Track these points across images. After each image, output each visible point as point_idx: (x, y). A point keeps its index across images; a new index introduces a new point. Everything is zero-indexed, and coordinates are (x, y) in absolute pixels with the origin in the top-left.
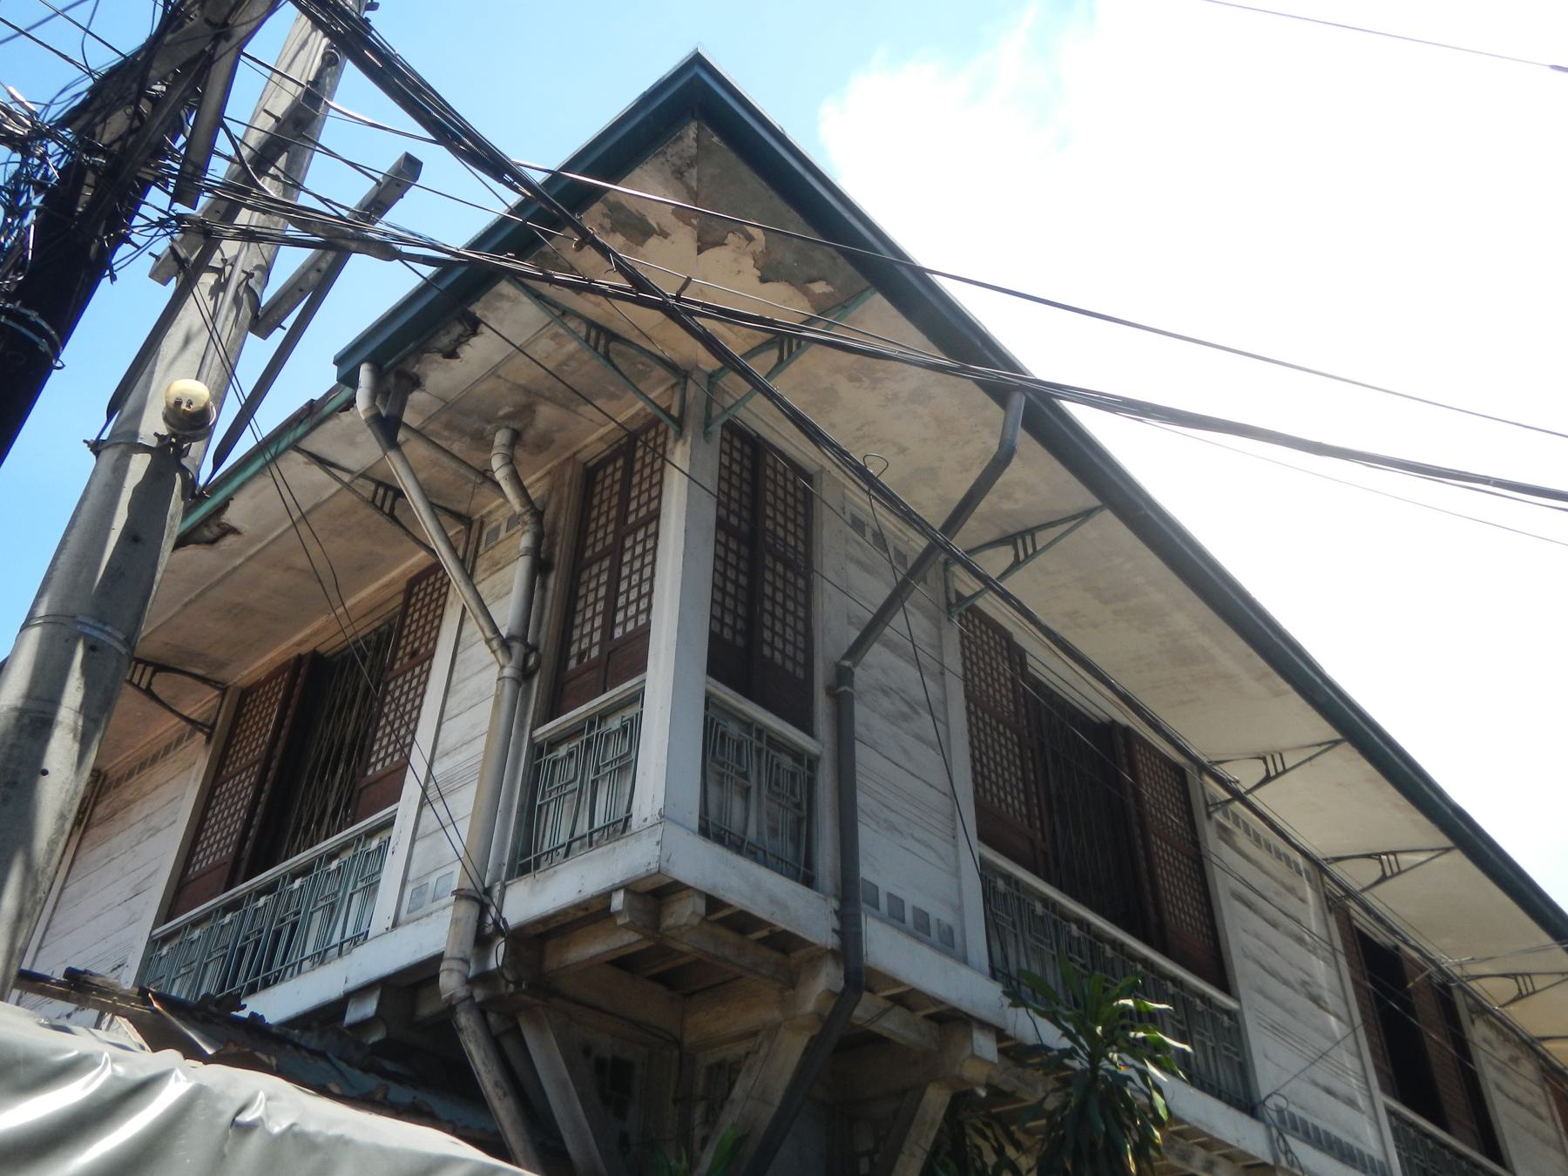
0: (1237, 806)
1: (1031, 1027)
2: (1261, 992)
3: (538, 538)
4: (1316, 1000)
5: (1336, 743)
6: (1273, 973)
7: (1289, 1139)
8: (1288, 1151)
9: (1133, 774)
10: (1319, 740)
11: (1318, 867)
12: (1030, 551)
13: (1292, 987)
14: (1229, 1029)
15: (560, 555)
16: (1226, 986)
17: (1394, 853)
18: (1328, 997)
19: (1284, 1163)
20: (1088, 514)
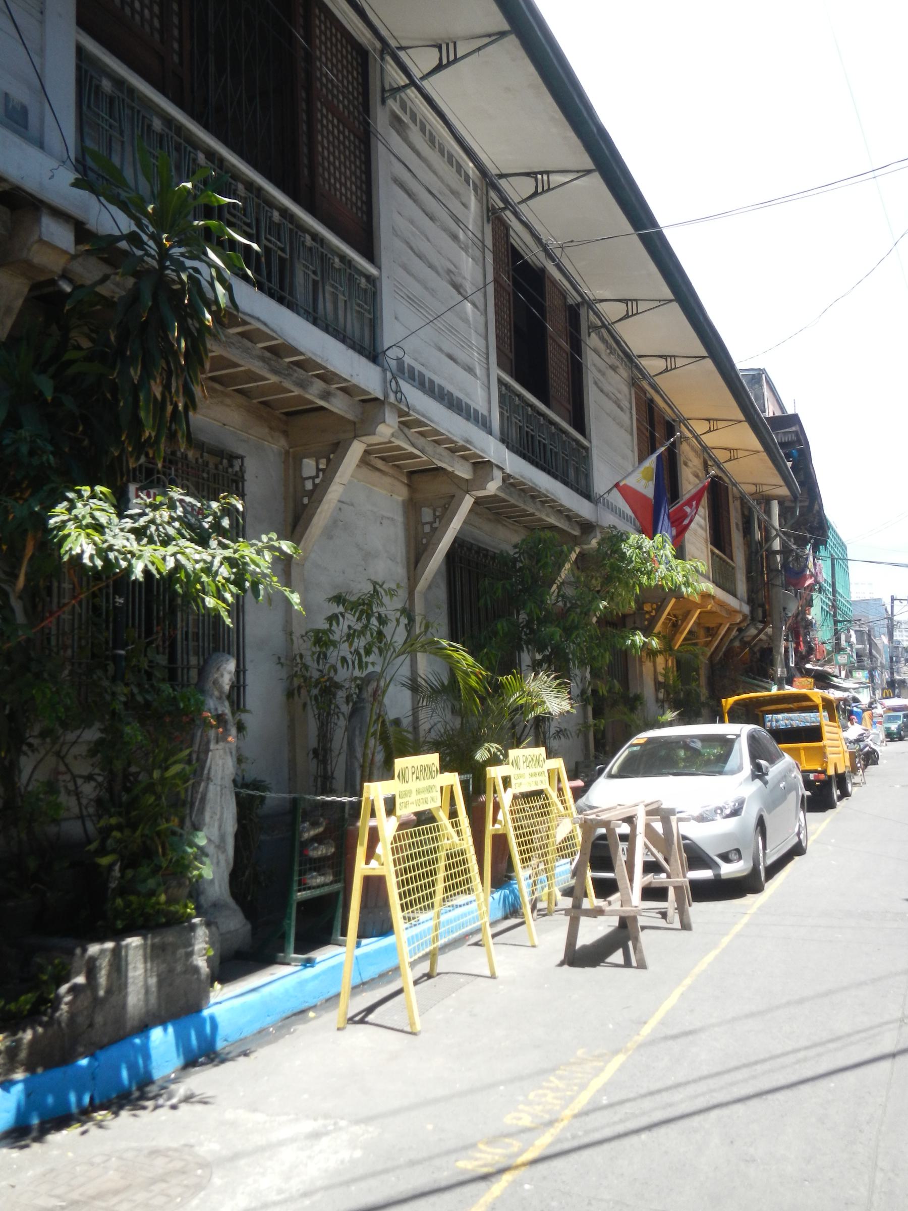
0: (412, 92)
1: (110, 221)
2: (405, 268)
5: (502, 34)
6: (420, 256)
7: (401, 382)
8: (398, 391)
9: (308, 37)
10: (579, 169)
11: (489, 181)
12: (452, 58)
13: (437, 272)
14: (365, 291)
16: (370, 254)
17: (548, 173)
18: (469, 288)
19: (392, 398)
20: (704, 357)
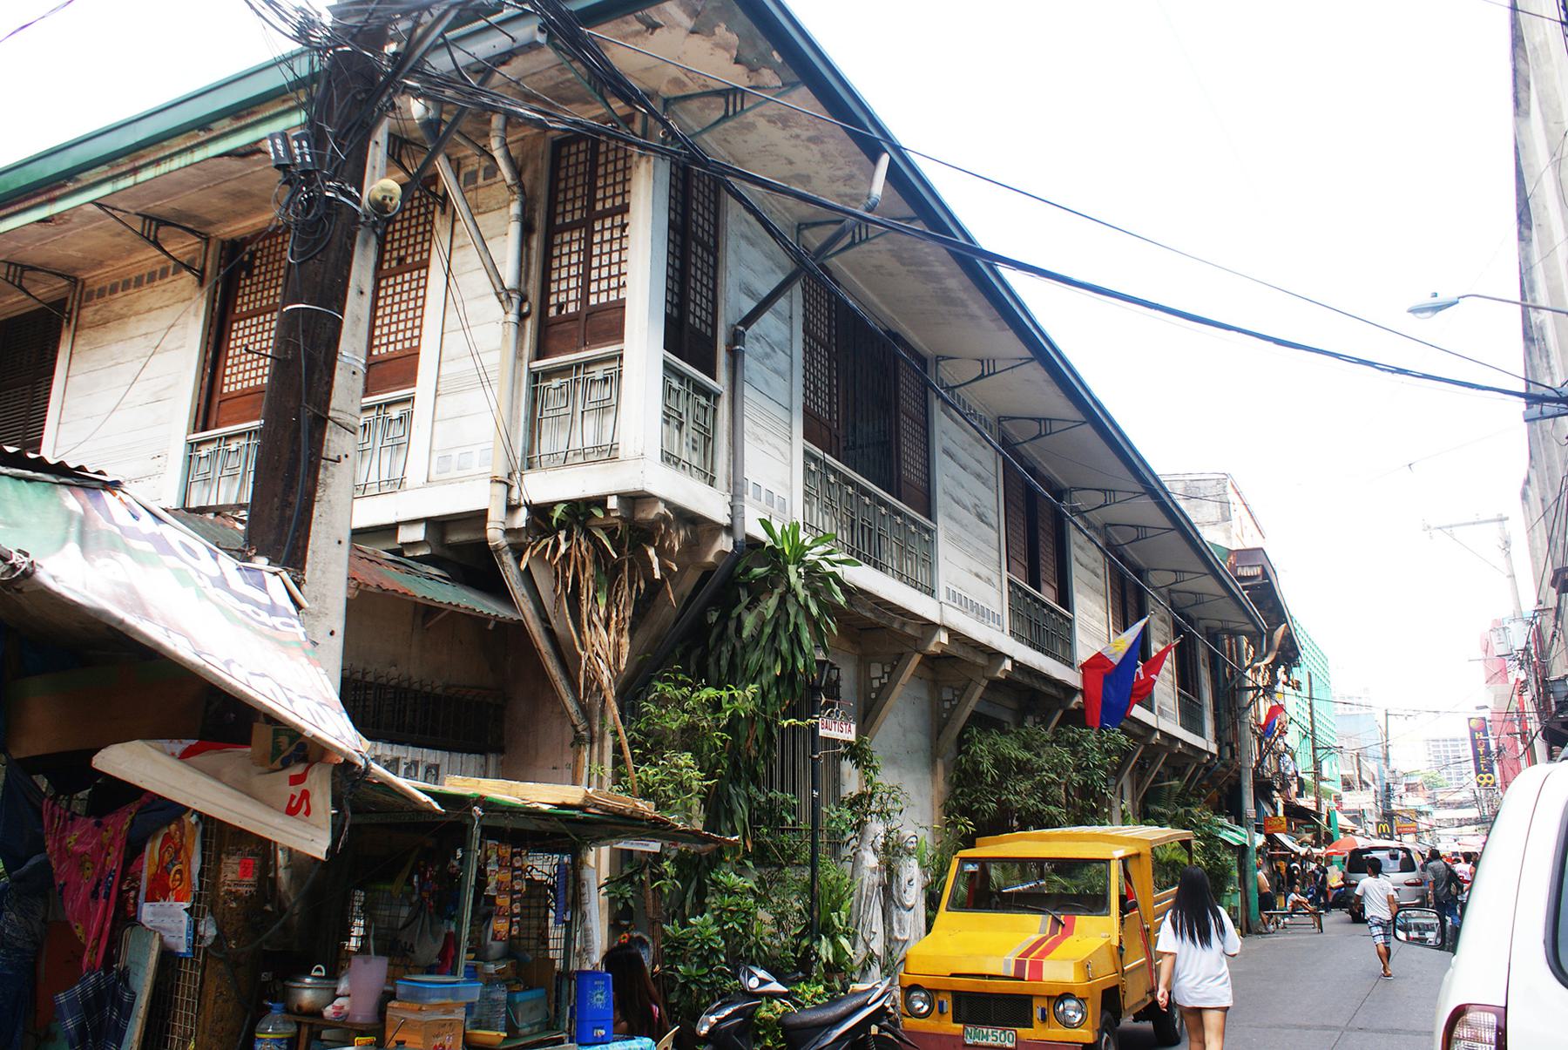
3: (524, 206)
4: (981, 517)
15: (539, 222)
